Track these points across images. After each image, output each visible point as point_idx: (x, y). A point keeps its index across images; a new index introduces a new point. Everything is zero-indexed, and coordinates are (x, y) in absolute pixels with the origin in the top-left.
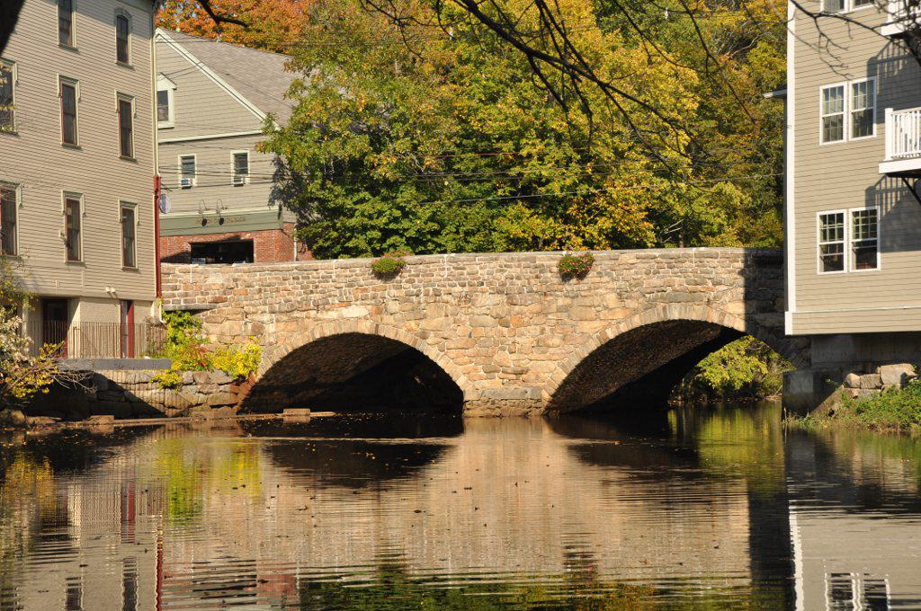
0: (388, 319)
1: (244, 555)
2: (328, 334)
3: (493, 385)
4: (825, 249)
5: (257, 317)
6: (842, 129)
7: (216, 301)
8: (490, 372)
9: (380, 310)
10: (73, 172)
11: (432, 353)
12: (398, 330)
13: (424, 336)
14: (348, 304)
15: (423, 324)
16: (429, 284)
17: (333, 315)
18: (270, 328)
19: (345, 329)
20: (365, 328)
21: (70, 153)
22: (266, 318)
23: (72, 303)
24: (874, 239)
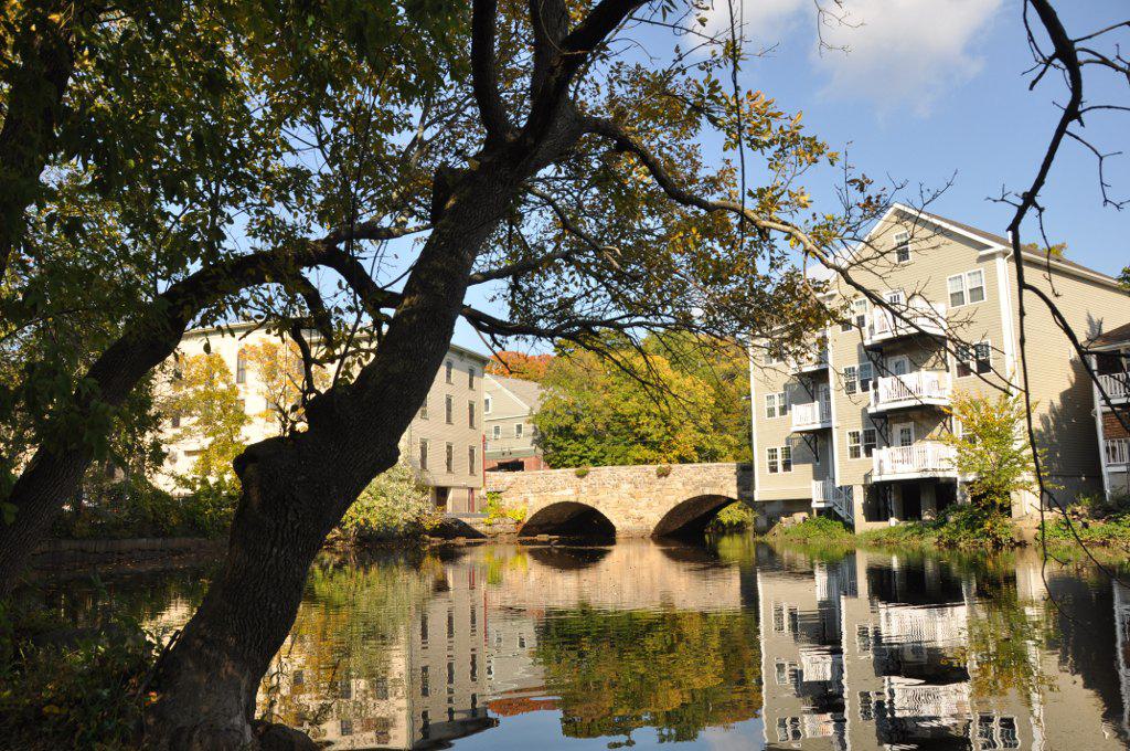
3: (629, 524)
4: (770, 464)
9: (579, 491)
11: (602, 510)
12: (586, 499)
13: (598, 502)
17: (558, 493)
20: (573, 499)
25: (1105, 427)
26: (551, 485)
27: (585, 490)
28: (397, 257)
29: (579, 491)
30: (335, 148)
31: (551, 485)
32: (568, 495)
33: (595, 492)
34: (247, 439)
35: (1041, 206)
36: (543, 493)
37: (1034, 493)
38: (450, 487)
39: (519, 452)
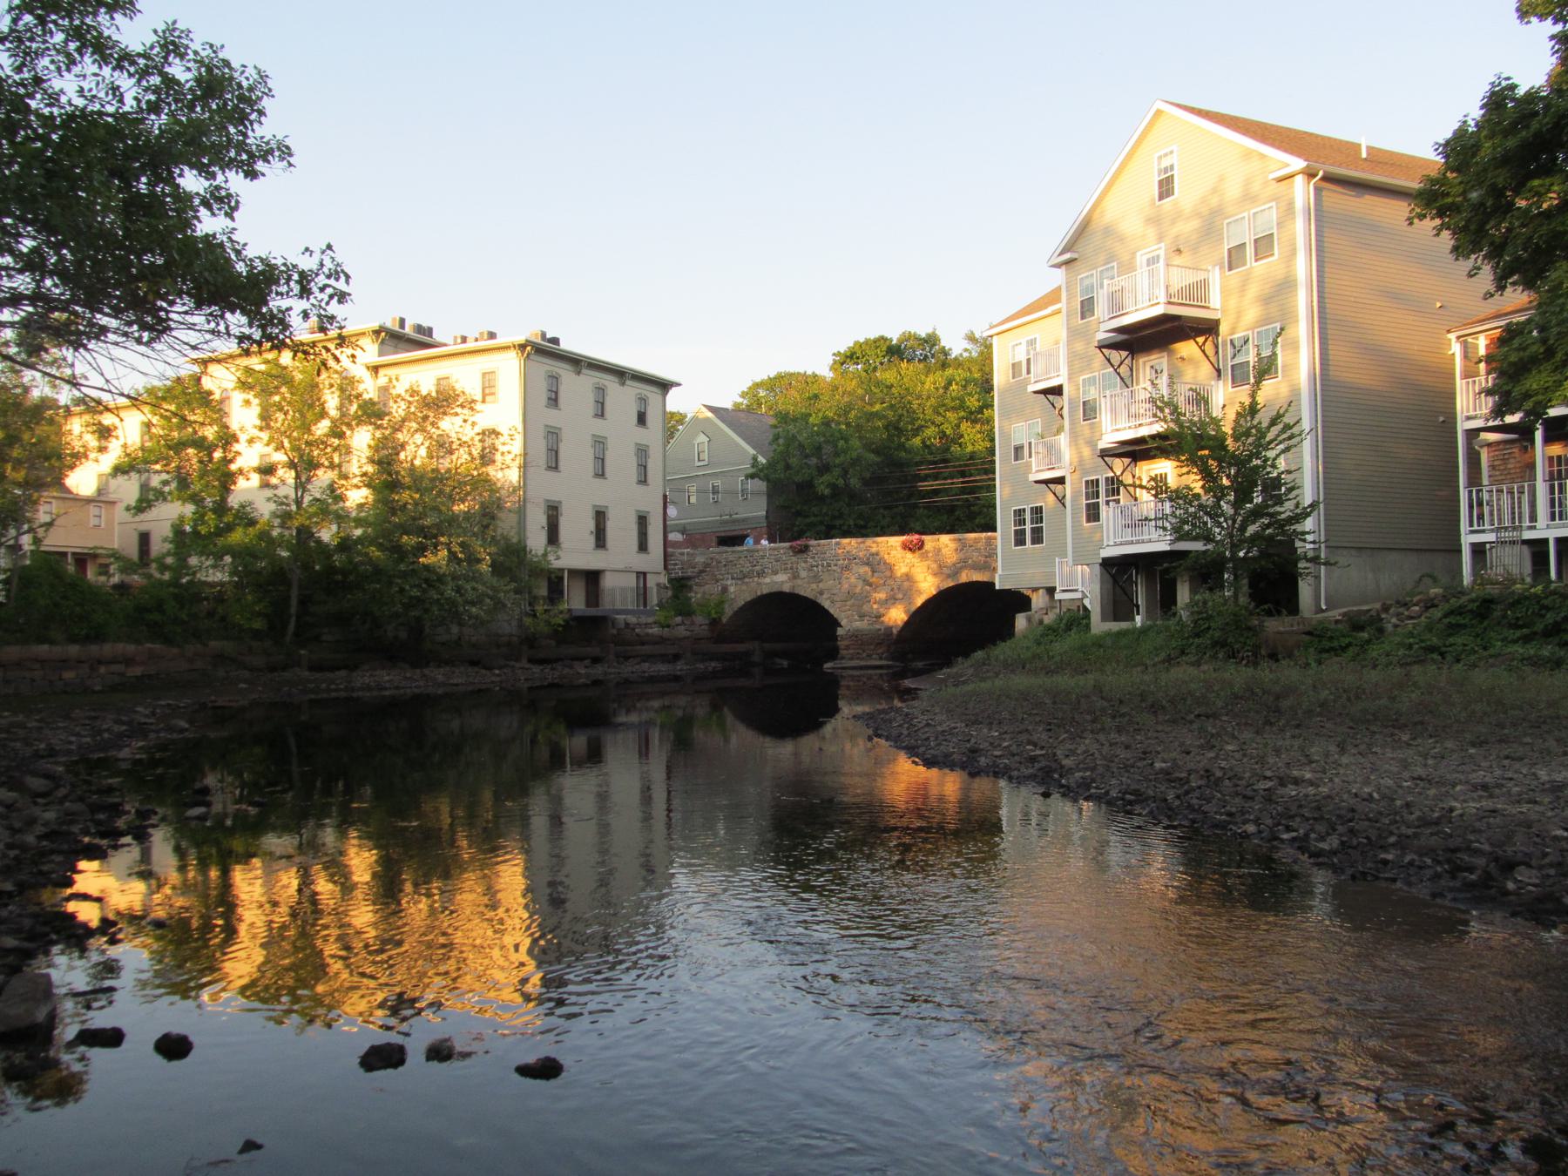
0: (799, 582)
1: (498, 457)
2: (765, 592)
3: (859, 625)
4: (1016, 531)
5: (724, 582)
6: (1153, 437)
7: (701, 572)
8: (862, 616)
9: (795, 576)
10: (601, 493)
11: (826, 604)
12: (806, 590)
13: (821, 593)
14: (775, 573)
15: (821, 585)
16: (823, 559)
17: (767, 580)
18: (732, 589)
19: (774, 590)
20: (786, 588)
21: (641, 430)
22: (729, 582)
23: (602, 576)
24: (69, 556)
25: (1493, 467)
26: (757, 568)
27: (803, 574)
28: (487, 1052)
29: (795, 576)
30: (231, 85)
31: (757, 568)
32: (780, 581)
33: (817, 579)
34: (172, 1004)
35: (96, 894)
36: (747, 580)
37: (1035, 590)
38: (603, 571)
39: (744, 520)
